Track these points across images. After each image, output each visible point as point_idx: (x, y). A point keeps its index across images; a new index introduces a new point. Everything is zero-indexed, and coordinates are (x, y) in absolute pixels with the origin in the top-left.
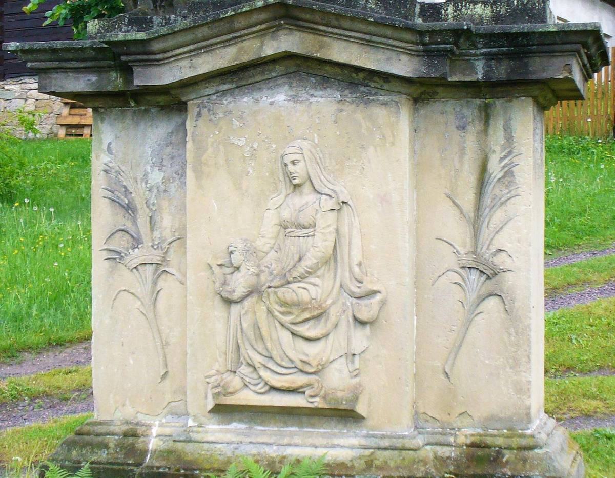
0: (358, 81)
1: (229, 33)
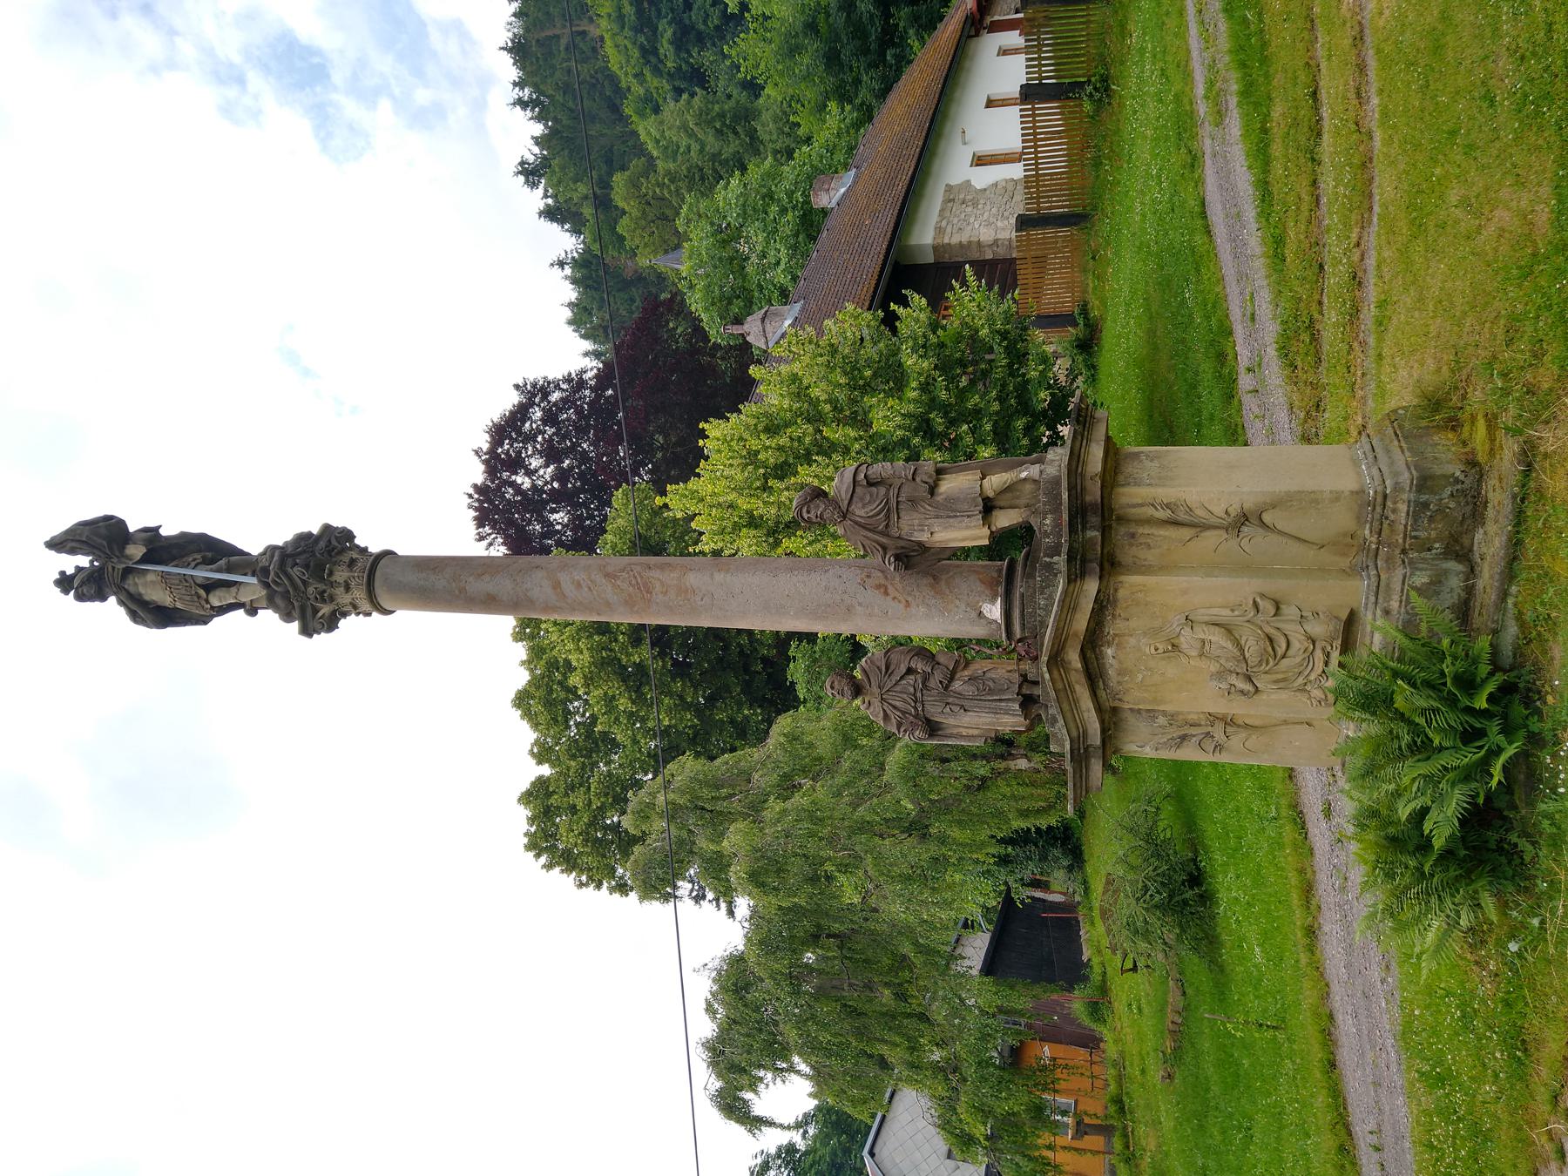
0: (1102, 606)
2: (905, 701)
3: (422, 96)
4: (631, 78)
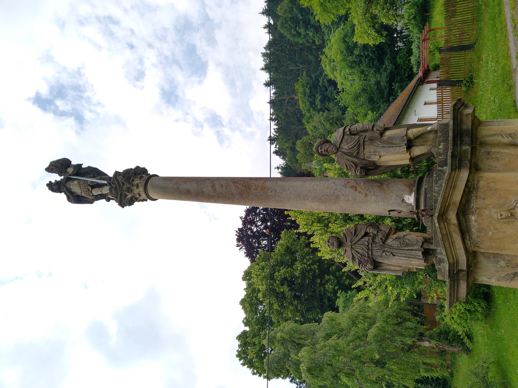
0: (469, 191)
2: (363, 249)
3: (248, 130)
4: (306, 111)
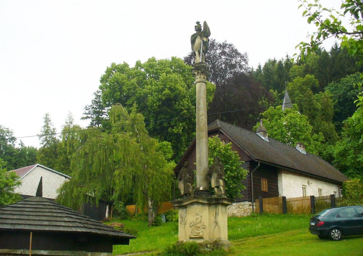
0: (203, 204)
1: (190, 199)
